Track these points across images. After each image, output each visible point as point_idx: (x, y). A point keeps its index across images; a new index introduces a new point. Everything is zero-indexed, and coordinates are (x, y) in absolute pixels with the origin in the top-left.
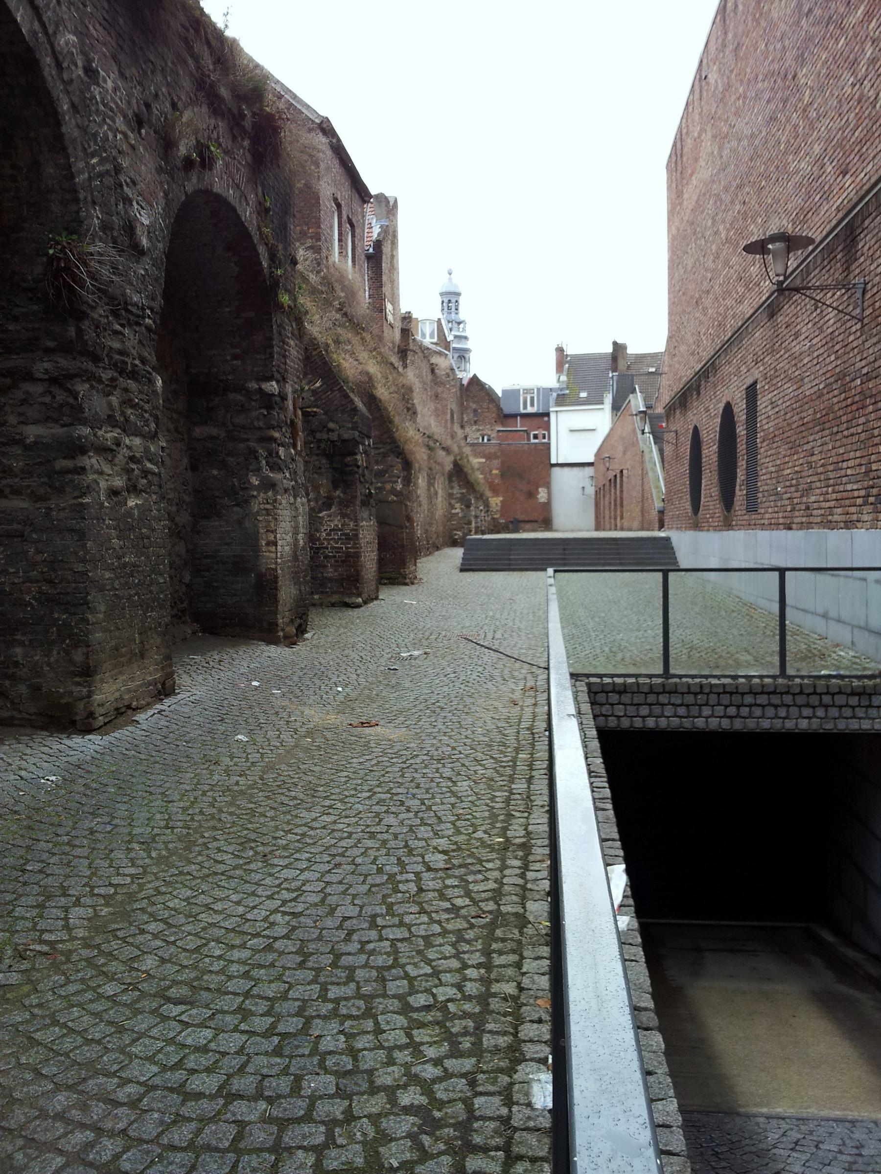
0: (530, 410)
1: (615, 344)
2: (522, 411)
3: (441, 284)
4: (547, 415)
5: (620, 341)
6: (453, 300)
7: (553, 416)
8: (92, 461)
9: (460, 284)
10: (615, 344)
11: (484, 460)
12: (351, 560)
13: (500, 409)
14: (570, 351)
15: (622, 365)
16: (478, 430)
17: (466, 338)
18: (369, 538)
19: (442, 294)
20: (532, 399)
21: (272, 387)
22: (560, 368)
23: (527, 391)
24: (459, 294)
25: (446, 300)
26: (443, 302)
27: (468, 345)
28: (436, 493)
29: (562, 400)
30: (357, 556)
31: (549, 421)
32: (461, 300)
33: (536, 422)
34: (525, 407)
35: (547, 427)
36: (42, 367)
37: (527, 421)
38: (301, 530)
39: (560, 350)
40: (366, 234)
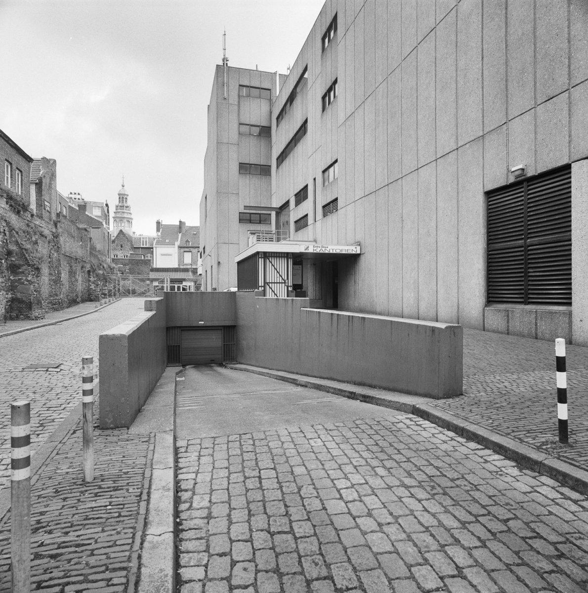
0: (145, 246)
1: (180, 222)
2: (142, 246)
3: (118, 189)
4: (152, 248)
5: (182, 221)
7: (154, 249)
9: (127, 190)
10: (180, 222)
11: (122, 266)
13: (132, 245)
14: (165, 222)
15: (184, 230)
16: (122, 253)
18: (360, 390)
19: (119, 194)
20: (146, 241)
22: (158, 230)
23: (143, 238)
24: (128, 195)
25: (121, 197)
26: (120, 198)
28: (77, 280)
29: (158, 243)
31: (153, 251)
32: (128, 198)
33: (147, 251)
39: (158, 223)
40: (31, 170)
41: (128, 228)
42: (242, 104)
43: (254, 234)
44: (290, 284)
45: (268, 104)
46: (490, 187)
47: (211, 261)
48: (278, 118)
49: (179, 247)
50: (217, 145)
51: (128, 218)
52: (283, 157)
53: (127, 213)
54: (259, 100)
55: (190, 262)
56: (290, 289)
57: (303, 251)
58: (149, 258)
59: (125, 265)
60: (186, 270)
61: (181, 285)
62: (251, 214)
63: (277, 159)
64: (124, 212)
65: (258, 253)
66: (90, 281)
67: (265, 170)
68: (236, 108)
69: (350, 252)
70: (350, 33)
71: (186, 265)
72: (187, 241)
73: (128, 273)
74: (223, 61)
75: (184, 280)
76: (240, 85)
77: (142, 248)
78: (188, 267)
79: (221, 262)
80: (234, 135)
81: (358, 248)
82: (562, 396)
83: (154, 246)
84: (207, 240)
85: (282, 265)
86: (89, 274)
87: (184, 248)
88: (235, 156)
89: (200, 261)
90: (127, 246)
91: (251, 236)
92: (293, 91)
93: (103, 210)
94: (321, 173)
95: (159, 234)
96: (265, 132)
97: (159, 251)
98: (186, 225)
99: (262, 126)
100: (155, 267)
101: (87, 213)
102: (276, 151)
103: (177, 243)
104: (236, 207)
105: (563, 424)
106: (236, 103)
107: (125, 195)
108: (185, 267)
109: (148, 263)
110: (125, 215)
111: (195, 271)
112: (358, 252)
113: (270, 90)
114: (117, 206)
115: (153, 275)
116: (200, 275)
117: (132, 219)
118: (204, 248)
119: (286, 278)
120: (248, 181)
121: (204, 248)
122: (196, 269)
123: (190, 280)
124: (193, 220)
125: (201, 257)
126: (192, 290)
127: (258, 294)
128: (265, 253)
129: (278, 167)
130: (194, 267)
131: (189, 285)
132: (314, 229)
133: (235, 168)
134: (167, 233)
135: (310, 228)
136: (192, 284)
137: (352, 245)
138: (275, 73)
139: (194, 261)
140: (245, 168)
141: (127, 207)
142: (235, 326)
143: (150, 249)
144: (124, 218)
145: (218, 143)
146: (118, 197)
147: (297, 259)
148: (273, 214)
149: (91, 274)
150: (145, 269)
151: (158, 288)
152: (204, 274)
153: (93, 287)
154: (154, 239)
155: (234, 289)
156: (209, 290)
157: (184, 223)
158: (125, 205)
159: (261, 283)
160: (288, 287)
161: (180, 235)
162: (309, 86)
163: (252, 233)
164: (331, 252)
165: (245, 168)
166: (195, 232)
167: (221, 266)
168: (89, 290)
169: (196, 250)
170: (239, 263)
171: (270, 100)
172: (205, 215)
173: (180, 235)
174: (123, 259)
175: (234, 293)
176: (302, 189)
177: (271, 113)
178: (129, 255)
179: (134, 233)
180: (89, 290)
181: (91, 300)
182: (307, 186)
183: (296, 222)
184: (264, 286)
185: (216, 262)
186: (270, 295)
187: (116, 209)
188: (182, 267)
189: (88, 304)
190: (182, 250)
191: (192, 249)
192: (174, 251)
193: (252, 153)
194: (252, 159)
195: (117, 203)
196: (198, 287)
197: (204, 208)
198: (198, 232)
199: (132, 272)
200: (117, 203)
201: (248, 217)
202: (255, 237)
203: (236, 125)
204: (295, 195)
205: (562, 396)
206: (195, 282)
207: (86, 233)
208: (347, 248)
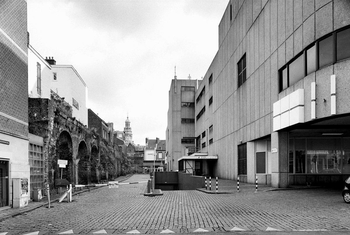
0: (140, 150)
1: (157, 138)
2: (139, 150)
4: (144, 151)
5: (158, 138)
6: (128, 123)
7: (145, 151)
8: (88, 168)
9: (130, 120)
10: (157, 138)
12: (105, 176)
14: (150, 138)
15: (158, 142)
17: (131, 132)
19: (126, 122)
20: (141, 148)
21: (97, 160)
22: (146, 142)
24: (130, 122)
26: (126, 124)
27: (132, 133)
28: (119, 167)
29: (147, 149)
30: (106, 176)
31: (144, 153)
33: (141, 153)
34: (140, 150)
35: (144, 153)
36: (85, 162)
37: (140, 152)
38: (250, 186)
39: (146, 139)
41: (130, 139)
42: (182, 94)
43: (187, 148)
44: (194, 169)
45: (193, 93)
46: (238, 144)
47: (170, 159)
48: (197, 100)
49: (156, 150)
50: (172, 112)
51: (130, 134)
52: (199, 117)
53: (130, 131)
54: (189, 92)
55: (161, 158)
56: (194, 171)
57: (198, 158)
58: (143, 156)
59: (132, 159)
60: (160, 162)
61: (157, 169)
62: (186, 139)
63: (197, 117)
64: (128, 131)
65: (183, 159)
66: (122, 167)
67: (192, 121)
68: (180, 96)
69: (214, 158)
70: (215, 83)
71: (160, 159)
72: (160, 148)
73: (133, 163)
74: (175, 77)
75: (159, 166)
76: (181, 87)
77: (139, 151)
78: (161, 160)
79: (174, 159)
80: (179, 108)
81: (217, 157)
82: (217, 185)
83: (145, 150)
84: (168, 148)
85: (192, 164)
86: (122, 165)
87: (159, 151)
88: (180, 116)
89: (166, 158)
90: (133, 151)
91: (186, 149)
92: (201, 92)
93: (123, 135)
94: (209, 128)
95: (147, 144)
96: (192, 105)
97: (147, 152)
98: (160, 139)
99: (191, 103)
100: (145, 160)
101: (117, 137)
102: (197, 114)
103: (156, 149)
104: (180, 138)
105: (210, 188)
106: (180, 94)
107: (128, 122)
108: (159, 160)
109: (142, 158)
110: (129, 133)
111: (164, 162)
112: (217, 158)
113: (194, 87)
114: (125, 128)
115: (145, 164)
116: (166, 164)
117: (132, 134)
118: (168, 152)
119: (192, 167)
120: (185, 126)
121: (168, 152)
122: (164, 161)
123: (162, 167)
124: (163, 137)
125: (166, 156)
126: (163, 171)
127: (184, 172)
128: (186, 159)
129: (197, 120)
130: (163, 160)
131: (161, 169)
132: (207, 147)
133: (179, 120)
134: (152, 143)
135: (206, 147)
136: (163, 168)
137: (215, 156)
138: (196, 80)
139: (163, 157)
140: (184, 121)
141: (129, 128)
142: (178, 184)
143: (143, 152)
144: (128, 134)
145: (173, 111)
146: (125, 123)
147: (196, 161)
148: (196, 140)
149: (123, 164)
150: (141, 161)
151: (147, 170)
152: (168, 164)
153: (123, 170)
154: (145, 147)
155: (178, 171)
156: (170, 171)
157: (159, 139)
158: (129, 127)
159: (184, 169)
160: (193, 170)
161: (157, 144)
162: (206, 94)
163: (186, 148)
164: (207, 158)
165: (184, 121)
166: (163, 143)
167: (174, 161)
168: (122, 171)
169: (164, 152)
170: (179, 161)
171: (194, 91)
172: (168, 137)
173: (157, 144)
174: (131, 157)
175: (178, 172)
176: (204, 133)
177: (195, 97)
178: (133, 155)
179: (133, 142)
180: (122, 171)
181: (123, 175)
182: (205, 131)
183: (202, 144)
184: (185, 170)
185: (172, 159)
186: (187, 172)
187: (124, 130)
188: (157, 160)
189: (122, 177)
190: (158, 152)
191: (162, 151)
192: (153, 152)
193: (187, 113)
194: (187, 117)
195: (125, 127)
196: (165, 169)
197: (167, 135)
198: (165, 143)
199: (135, 163)
200: (125, 127)
201: (185, 140)
202: (188, 149)
203: (180, 103)
204: (202, 134)
205: (217, 185)
206: (164, 167)
207: (121, 148)
208: (213, 157)
